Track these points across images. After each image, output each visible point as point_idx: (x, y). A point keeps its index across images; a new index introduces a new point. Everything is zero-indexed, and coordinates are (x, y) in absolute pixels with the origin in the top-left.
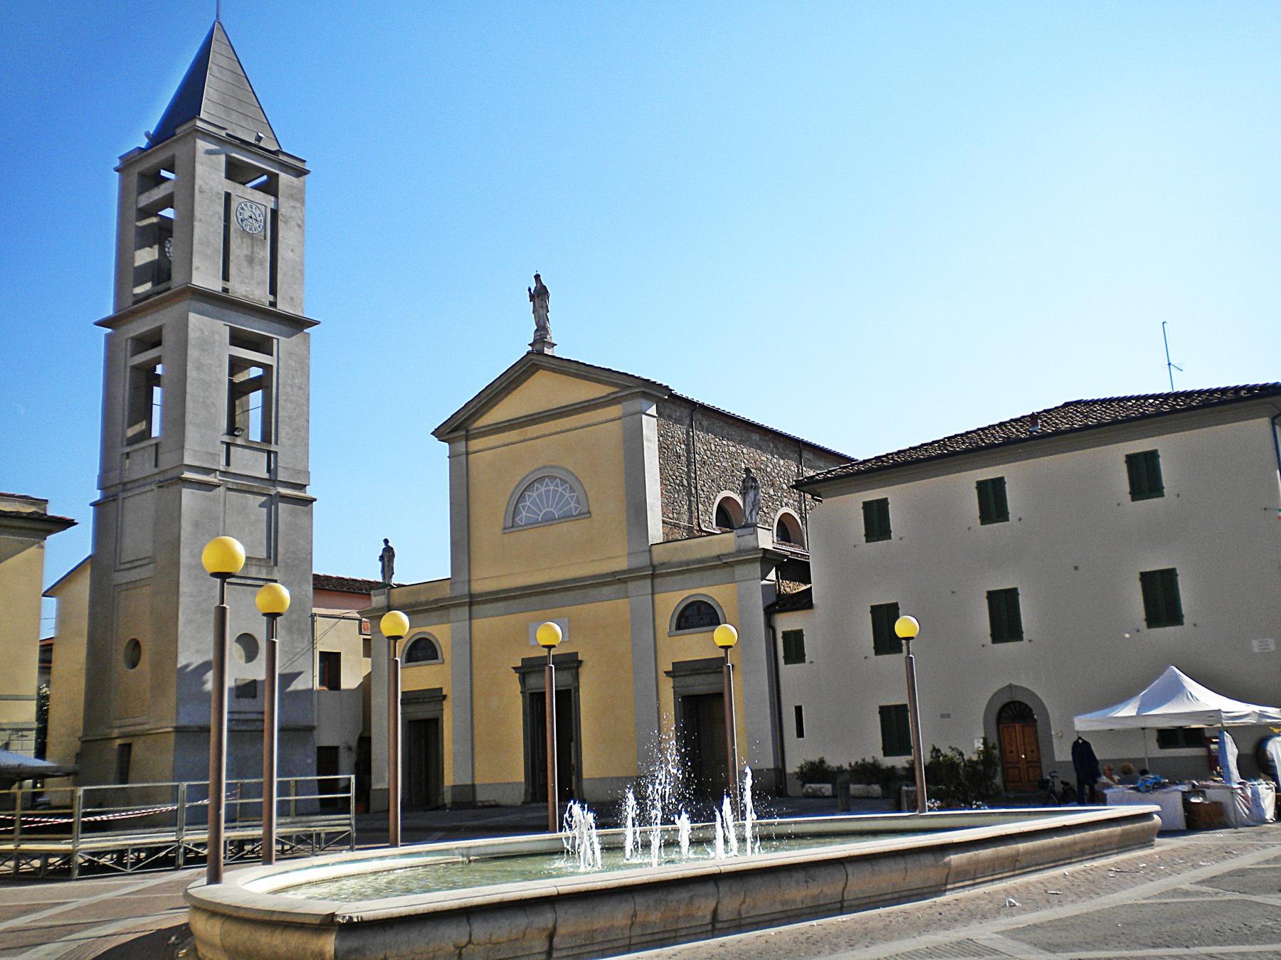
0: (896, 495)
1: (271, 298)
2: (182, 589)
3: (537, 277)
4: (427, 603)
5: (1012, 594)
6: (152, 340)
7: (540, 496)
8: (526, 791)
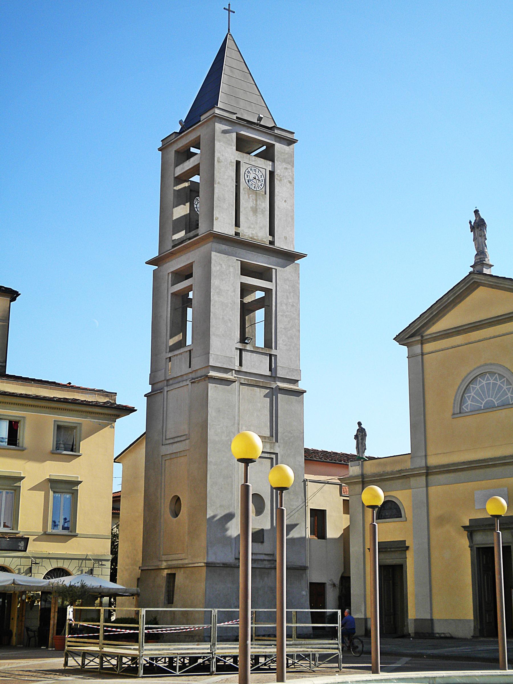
1: (270, 238)
3: (476, 212)
4: (392, 473)
6: (185, 274)
7: (482, 387)
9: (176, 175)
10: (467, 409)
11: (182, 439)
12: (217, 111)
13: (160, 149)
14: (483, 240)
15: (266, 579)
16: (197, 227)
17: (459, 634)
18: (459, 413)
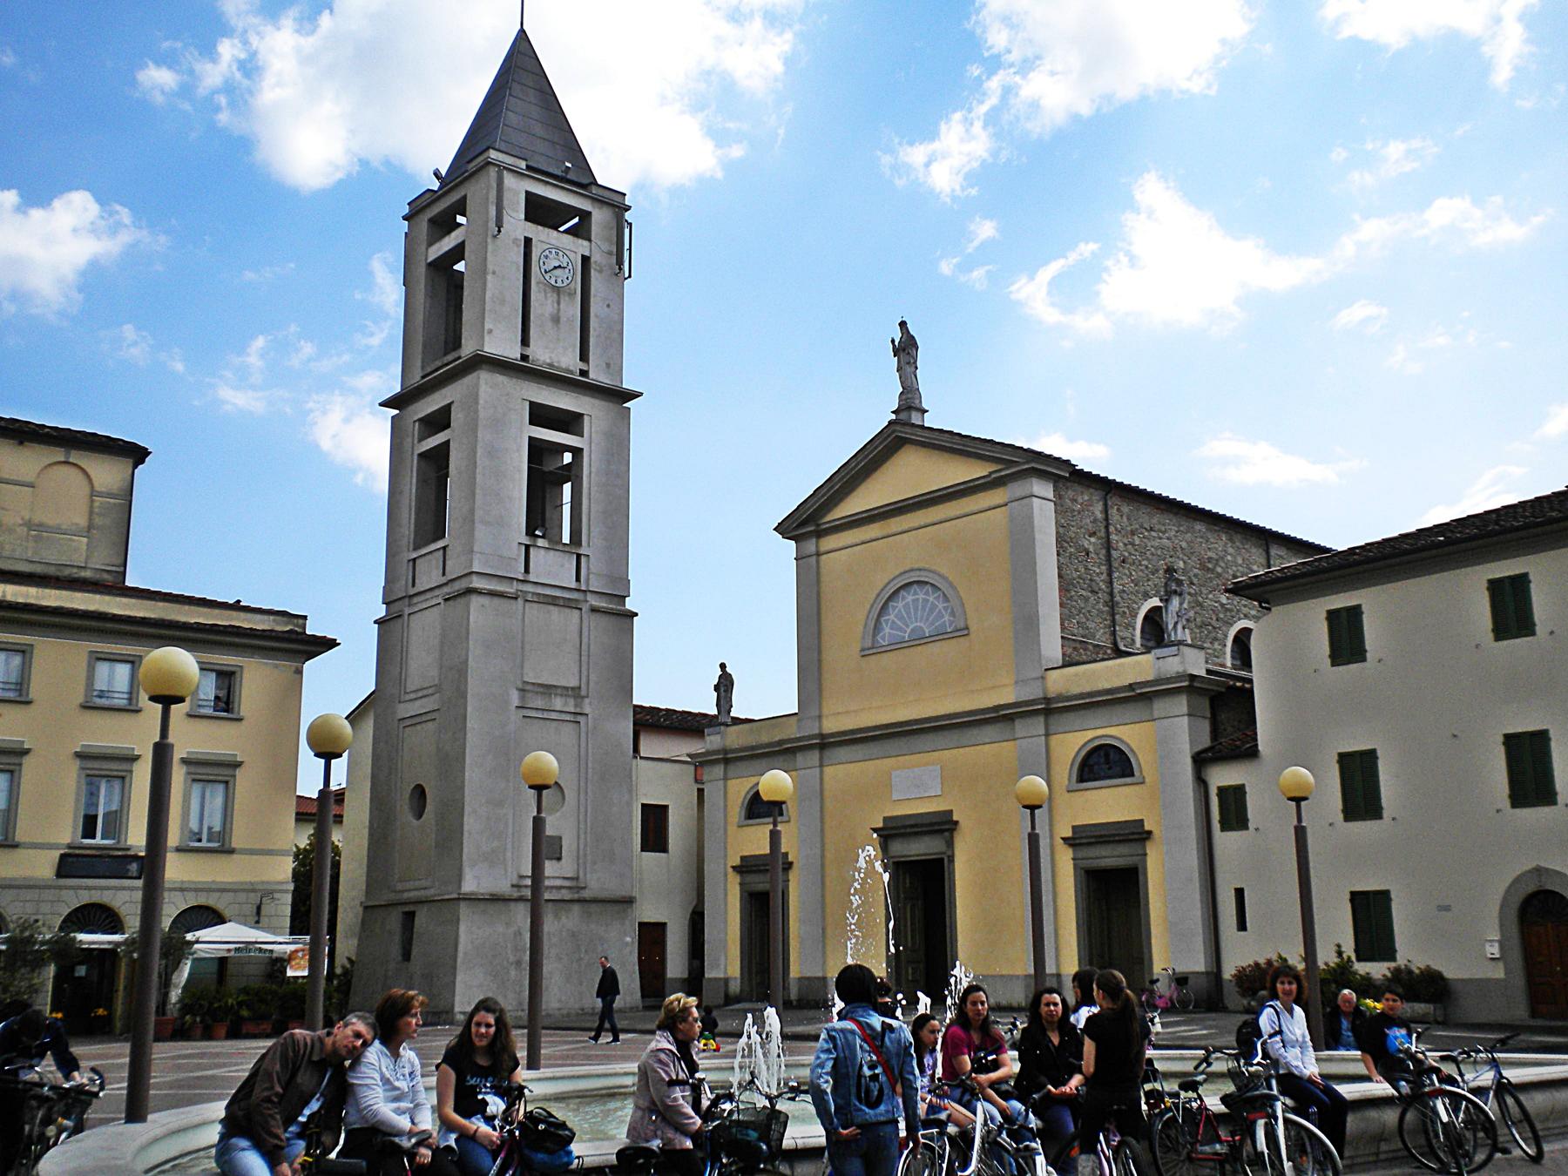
0: (1376, 605)
3: (903, 324)
5: (1369, 757)
6: (439, 421)
7: (906, 606)
12: (493, 154)
13: (405, 218)
16: (459, 346)
18: (963, 632)
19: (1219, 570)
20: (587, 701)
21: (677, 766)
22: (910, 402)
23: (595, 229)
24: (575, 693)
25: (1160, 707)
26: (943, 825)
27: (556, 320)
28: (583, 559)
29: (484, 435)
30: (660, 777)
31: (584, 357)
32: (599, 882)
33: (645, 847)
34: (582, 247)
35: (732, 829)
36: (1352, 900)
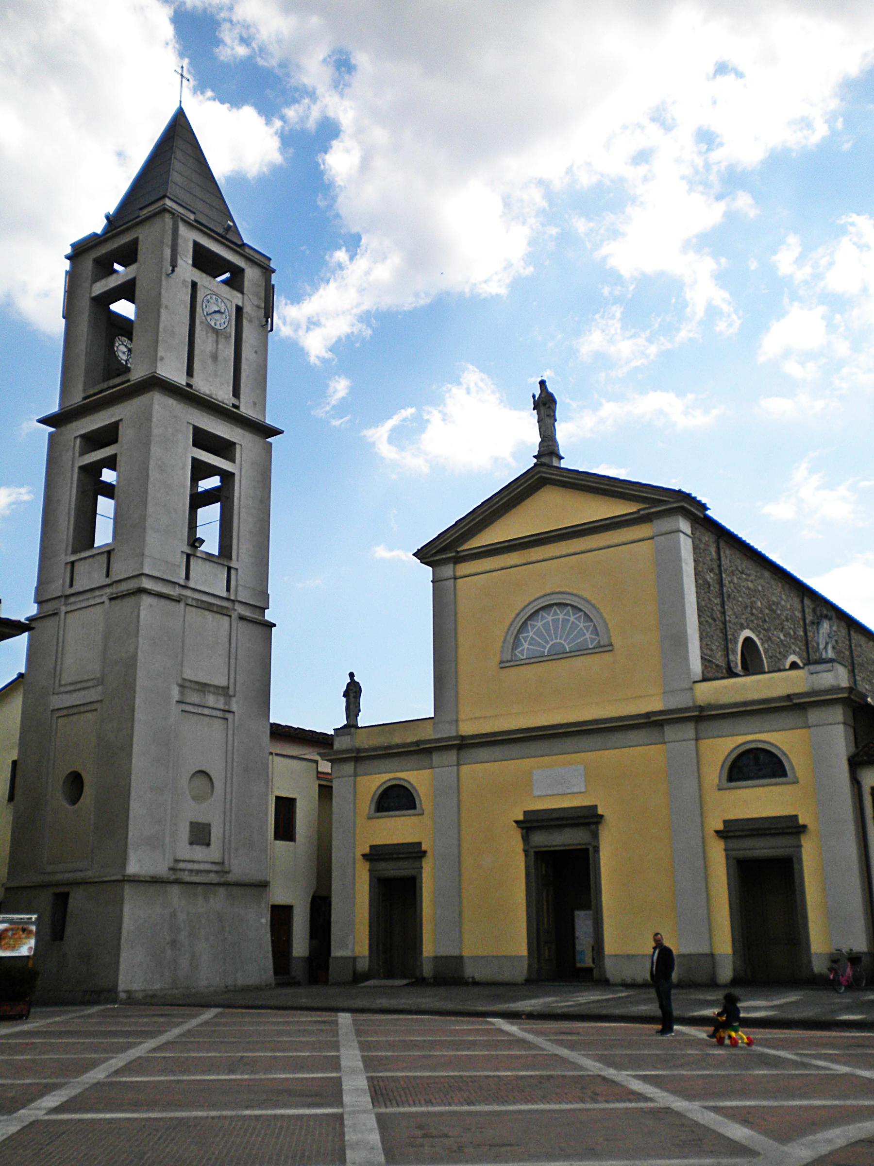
1: (234, 401)
2: (138, 715)
4: (404, 745)
6: (108, 436)
7: (566, 621)
8: (530, 966)
9: (93, 295)
10: (523, 655)
11: (90, 684)
12: (169, 203)
14: (552, 421)
15: (212, 900)
17: (506, 976)
18: (607, 648)
19: (779, 612)
20: (234, 700)
21: (304, 763)
22: (548, 449)
23: (247, 284)
24: (224, 691)
25: (814, 716)
26: (589, 819)
27: (215, 357)
28: (233, 572)
29: (156, 450)
30: (292, 777)
31: (236, 393)
32: (241, 867)
33: (277, 837)
34: (237, 298)
35: (360, 821)
36: (272, 911)
